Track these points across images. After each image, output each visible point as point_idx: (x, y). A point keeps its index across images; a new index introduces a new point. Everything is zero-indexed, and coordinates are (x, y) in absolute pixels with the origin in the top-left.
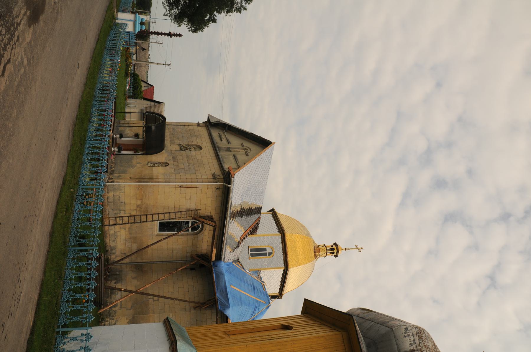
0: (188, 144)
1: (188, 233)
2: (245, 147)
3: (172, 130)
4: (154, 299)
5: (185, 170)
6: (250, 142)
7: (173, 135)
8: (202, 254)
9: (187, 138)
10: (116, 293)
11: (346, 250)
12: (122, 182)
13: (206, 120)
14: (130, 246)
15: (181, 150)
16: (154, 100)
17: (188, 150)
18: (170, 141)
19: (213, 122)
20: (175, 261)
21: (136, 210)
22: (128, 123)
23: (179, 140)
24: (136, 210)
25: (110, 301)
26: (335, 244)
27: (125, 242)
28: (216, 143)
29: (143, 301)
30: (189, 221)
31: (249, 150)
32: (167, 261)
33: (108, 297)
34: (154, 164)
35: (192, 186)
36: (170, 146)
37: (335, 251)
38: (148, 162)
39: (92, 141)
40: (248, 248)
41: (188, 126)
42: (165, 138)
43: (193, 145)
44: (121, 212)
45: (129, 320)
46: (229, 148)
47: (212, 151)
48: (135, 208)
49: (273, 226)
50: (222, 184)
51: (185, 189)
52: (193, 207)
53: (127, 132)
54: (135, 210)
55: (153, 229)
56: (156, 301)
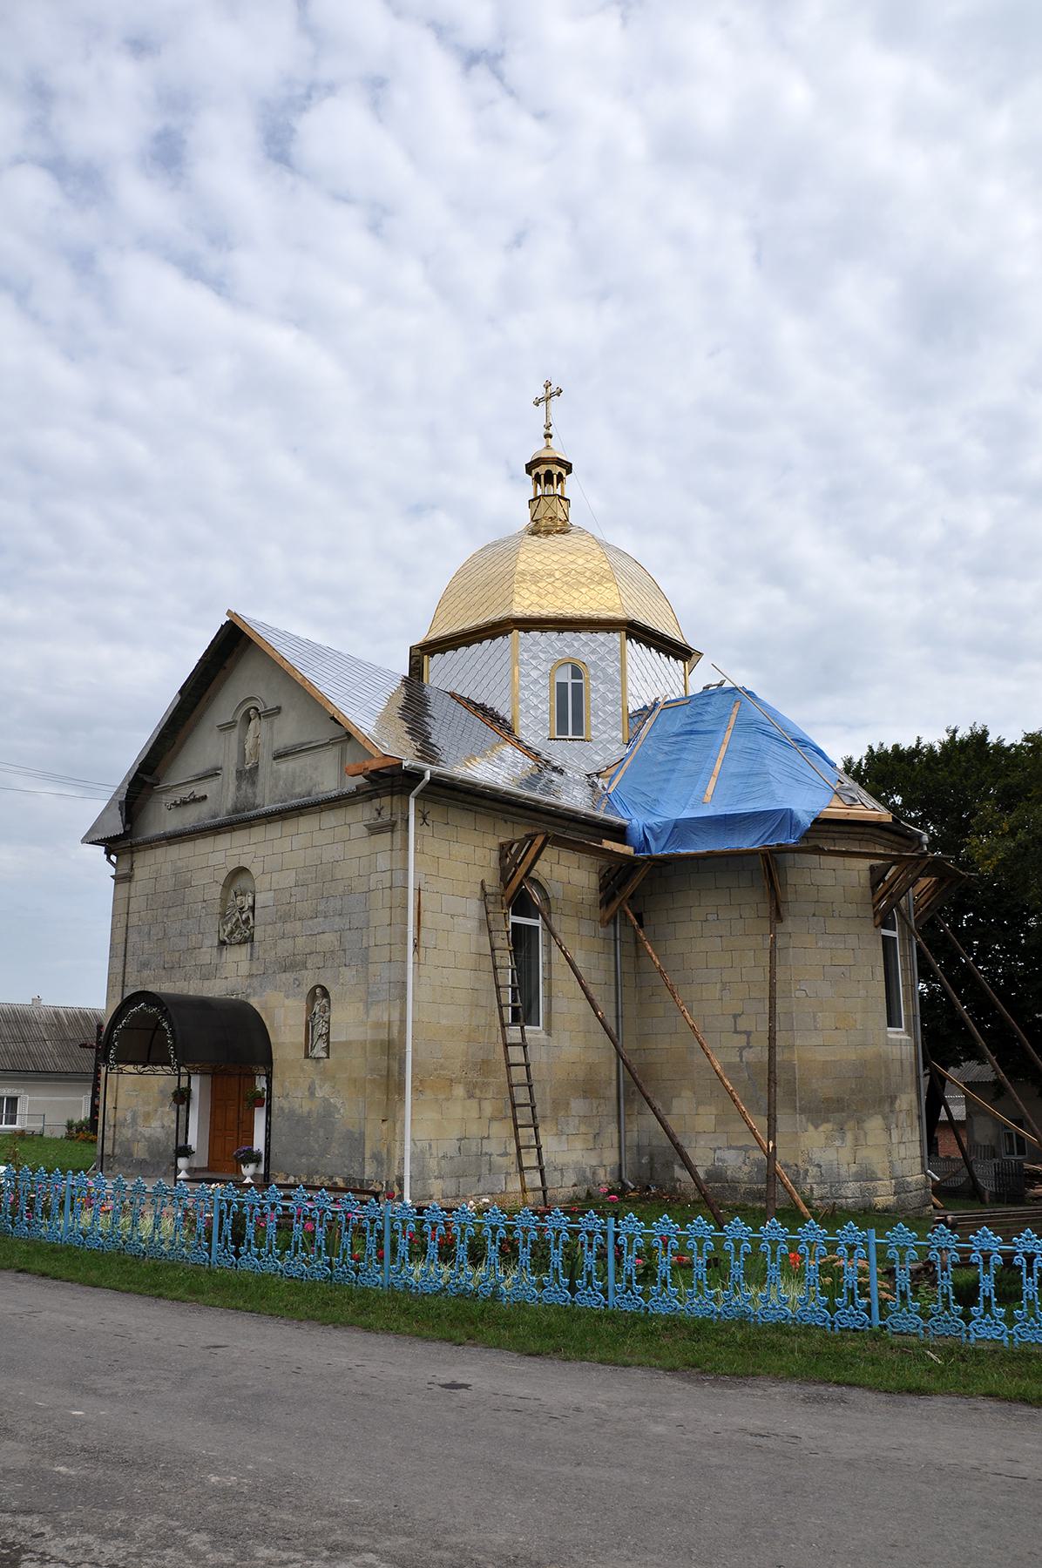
0: (218, 916)
1: (543, 929)
2: (238, 718)
3: (146, 973)
6: (210, 700)
8: (602, 888)
10: (720, 1164)
11: (551, 436)
12: (403, 1150)
13: (100, 850)
14: (577, 1120)
15: (249, 940)
18: (205, 978)
19: (124, 827)
20: (616, 975)
21: (480, 1099)
22: (115, 1126)
24: (480, 1099)
26: (530, 468)
27: (564, 1137)
28: (214, 817)
29: (749, 1078)
30: (512, 923)
31: (253, 704)
32: (617, 1003)
33: (735, 1189)
34: (315, 1032)
35: (417, 904)
36: (226, 978)
37: (557, 470)
38: (307, 1056)
39: (210, 1246)
40: (555, 739)
41: (128, 914)
43: (224, 900)
44: (484, 1151)
45: (809, 1124)
46: (240, 774)
47: (258, 833)
48: (473, 1103)
49: (479, 653)
50: (412, 801)
51: (422, 929)
52: (473, 907)
53: (159, 1130)
54: (480, 1105)
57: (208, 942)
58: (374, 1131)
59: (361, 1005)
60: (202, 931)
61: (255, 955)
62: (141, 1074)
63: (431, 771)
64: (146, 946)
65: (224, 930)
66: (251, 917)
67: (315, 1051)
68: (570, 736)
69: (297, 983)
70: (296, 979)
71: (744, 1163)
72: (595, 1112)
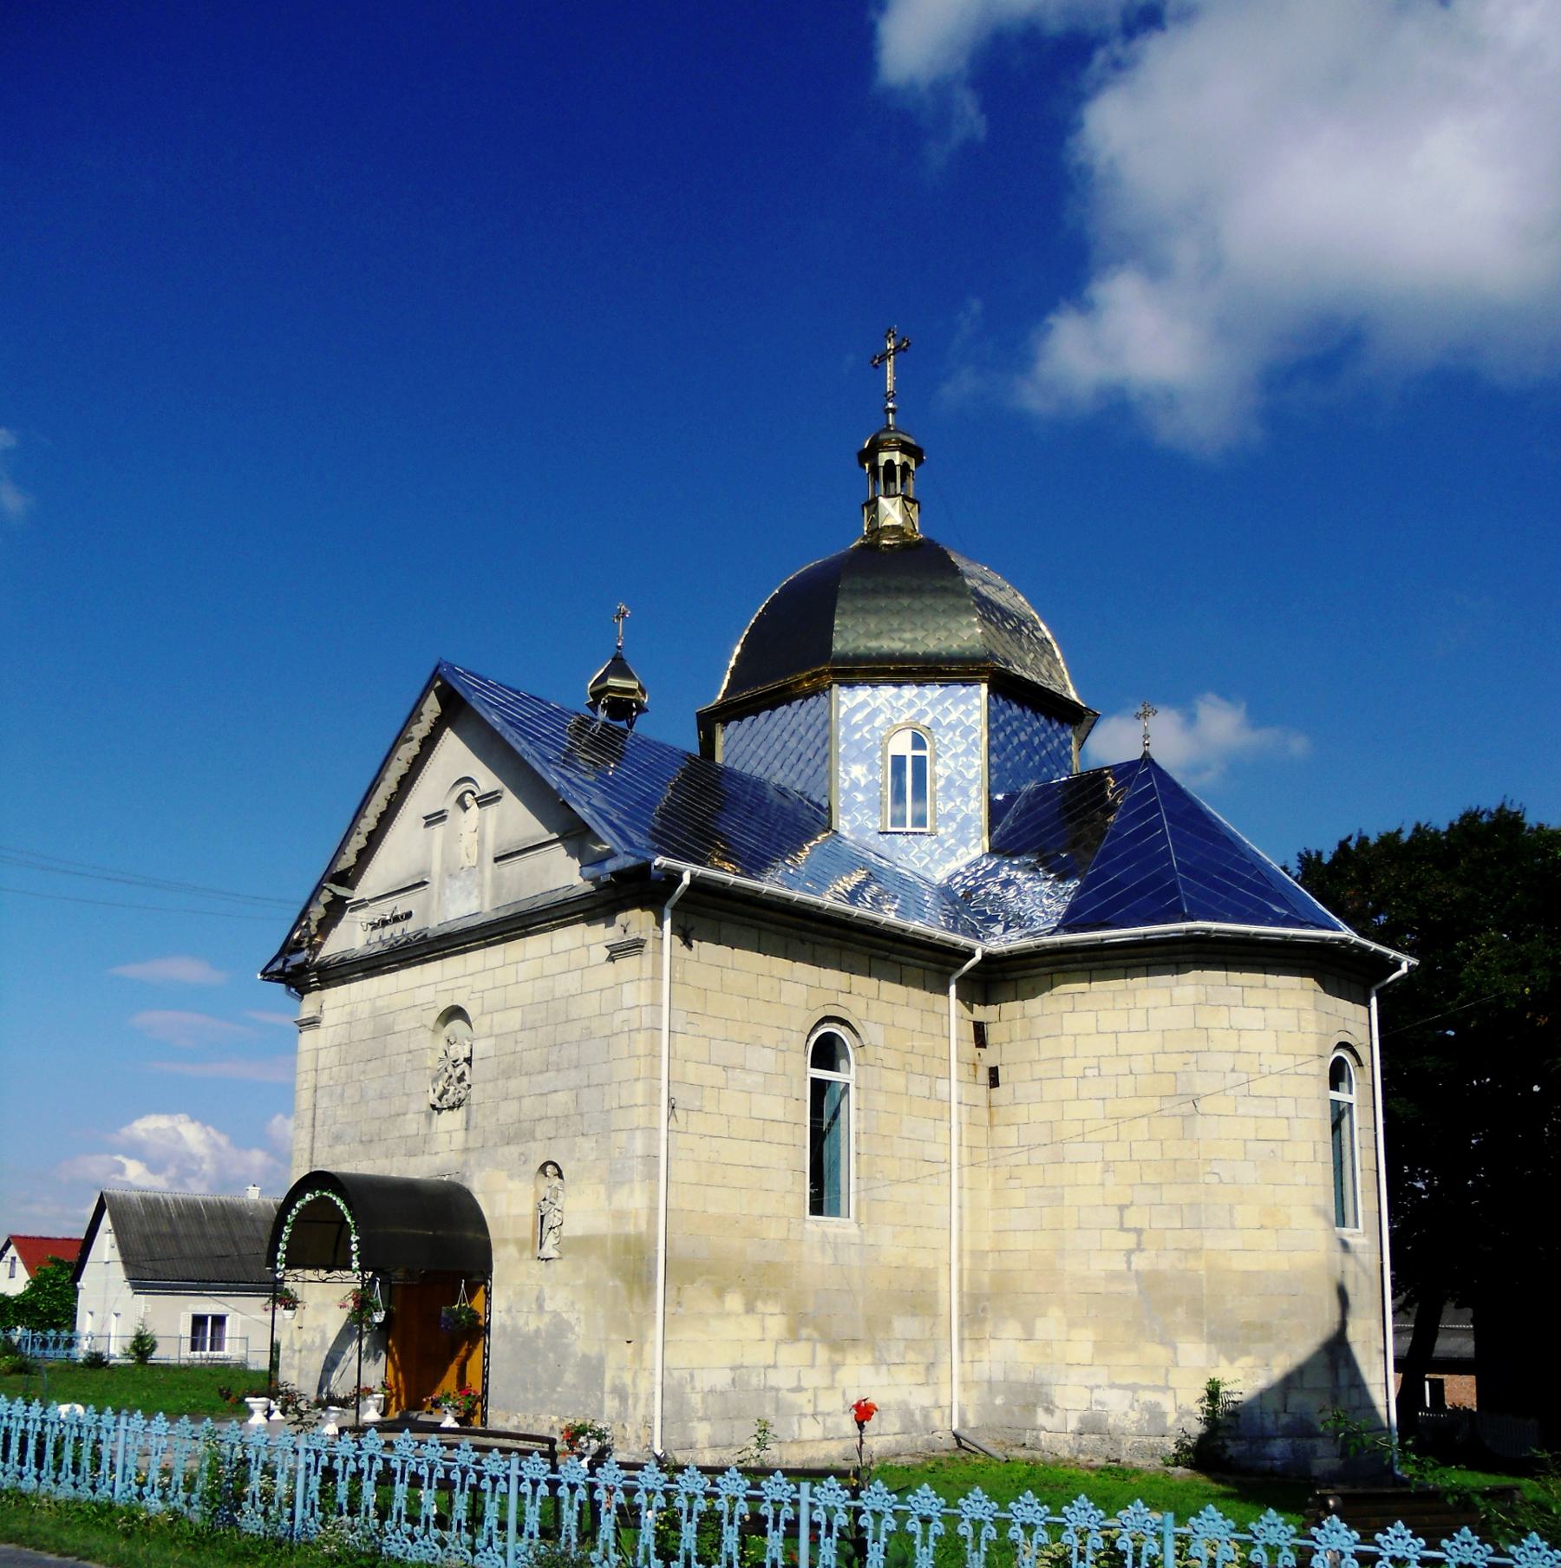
3: (339, 1149)
4: (1134, 1246)
5: (588, 1086)
7: (371, 1141)
9: (390, 1075)
16: (83, 1237)
17: (463, 1073)
18: (411, 1154)
23: (405, 1114)
25: (1132, 1435)
27: (884, 1368)
29: (1140, 1292)
30: (812, 1079)
41: (316, 1071)
42: (394, 1175)
50: (667, 912)
55: (839, 1241)
56: (1142, 1238)
57: (414, 1107)
58: (617, 1358)
59: (602, 1189)
60: (407, 1091)
61: (472, 1123)
62: (324, 1281)
63: (691, 871)
64: (338, 1113)
65: (434, 1091)
66: (467, 1073)
67: (544, 1249)
68: (909, 828)
69: (523, 1158)
70: (522, 1154)
71: (1131, 1407)
72: (928, 1334)
